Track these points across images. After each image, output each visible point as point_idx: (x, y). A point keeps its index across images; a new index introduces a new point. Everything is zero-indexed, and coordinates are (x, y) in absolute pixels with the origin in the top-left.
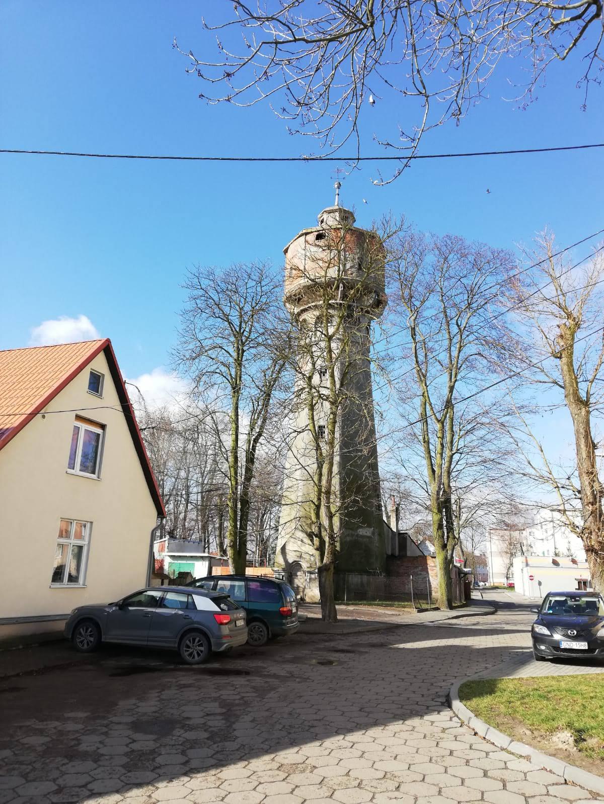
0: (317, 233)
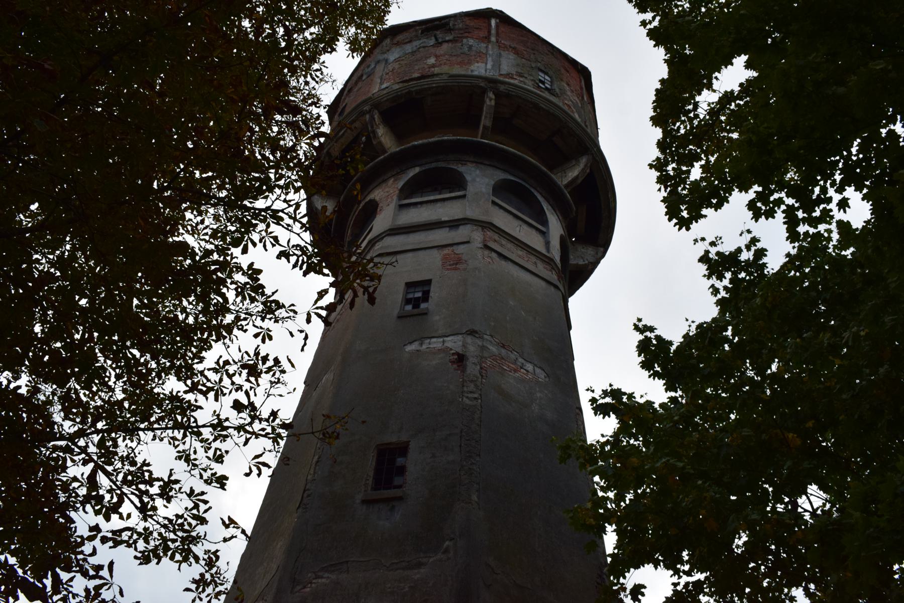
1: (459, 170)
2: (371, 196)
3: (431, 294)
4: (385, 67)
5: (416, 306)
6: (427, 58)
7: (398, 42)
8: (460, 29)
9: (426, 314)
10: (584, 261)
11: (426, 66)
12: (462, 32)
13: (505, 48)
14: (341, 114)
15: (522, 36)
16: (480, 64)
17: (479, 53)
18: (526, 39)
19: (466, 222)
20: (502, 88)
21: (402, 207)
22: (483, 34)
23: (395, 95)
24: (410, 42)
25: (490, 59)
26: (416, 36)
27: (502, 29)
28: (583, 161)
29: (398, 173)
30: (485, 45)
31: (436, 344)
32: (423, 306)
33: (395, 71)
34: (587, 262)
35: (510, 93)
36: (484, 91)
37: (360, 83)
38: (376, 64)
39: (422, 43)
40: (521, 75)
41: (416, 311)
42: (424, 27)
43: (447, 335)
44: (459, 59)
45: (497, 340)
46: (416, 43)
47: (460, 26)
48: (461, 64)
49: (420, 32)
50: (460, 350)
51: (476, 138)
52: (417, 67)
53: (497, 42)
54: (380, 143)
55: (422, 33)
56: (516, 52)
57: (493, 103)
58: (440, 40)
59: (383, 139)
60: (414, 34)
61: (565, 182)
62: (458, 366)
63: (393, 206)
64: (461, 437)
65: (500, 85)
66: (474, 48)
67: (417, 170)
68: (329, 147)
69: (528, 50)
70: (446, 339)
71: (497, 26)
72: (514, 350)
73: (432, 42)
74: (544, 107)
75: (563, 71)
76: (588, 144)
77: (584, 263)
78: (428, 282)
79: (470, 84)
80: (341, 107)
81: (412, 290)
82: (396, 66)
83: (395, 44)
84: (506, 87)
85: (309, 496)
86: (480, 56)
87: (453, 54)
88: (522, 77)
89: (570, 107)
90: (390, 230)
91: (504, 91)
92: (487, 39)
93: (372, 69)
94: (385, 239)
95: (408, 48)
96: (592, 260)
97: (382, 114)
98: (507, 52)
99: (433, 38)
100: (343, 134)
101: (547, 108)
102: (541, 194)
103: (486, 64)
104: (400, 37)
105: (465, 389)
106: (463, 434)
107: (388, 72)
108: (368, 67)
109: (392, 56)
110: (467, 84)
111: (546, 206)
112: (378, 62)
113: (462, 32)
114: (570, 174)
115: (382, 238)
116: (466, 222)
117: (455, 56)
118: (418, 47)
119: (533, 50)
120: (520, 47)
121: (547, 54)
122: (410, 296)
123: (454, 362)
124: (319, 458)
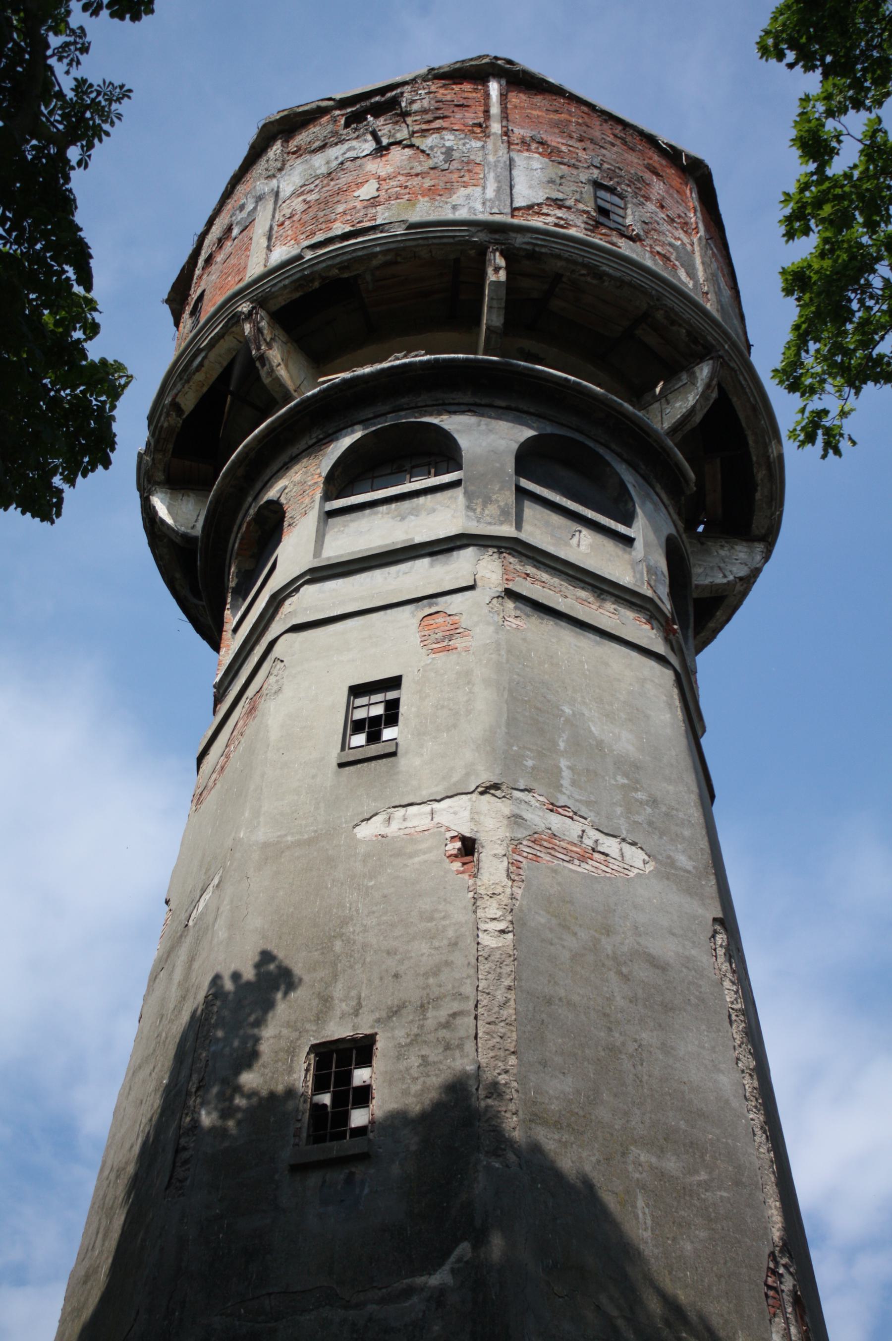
1: (446, 427)
2: (272, 494)
3: (403, 709)
4: (275, 209)
5: (374, 737)
6: (359, 185)
7: (299, 148)
8: (425, 111)
9: (394, 754)
10: (725, 576)
11: (359, 205)
12: (429, 117)
13: (525, 144)
14: (195, 312)
15: (556, 111)
16: (469, 190)
17: (468, 163)
18: (564, 116)
19: (465, 542)
20: (519, 240)
21: (332, 514)
22: (472, 117)
23: (299, 275)
24: (322, 148)
25: (491, 176)
26: (335, 133)
27: (517, 99)
28: (704, 371)
29: (320, 440)
30: (479, 144)
31: (418, 817)
32: (388, 733)
33: (296, 218)
34: (731, 578)
35: (537, 249)
36: (482, 253)
37: (229, 243)
38: (257, 202)
39: (349, 149)
40: (558, 203)
41: (375, 749)
42: (349, 110)
43: (438, 798)
44: (427, 183)
45: (541, 799)
46: (335, 153)
47: (425, 103)
48: (431, 192)
49: (343, 122)
50: (399, 980)
51: (475, 353)
52: (340, 208)
53: (506, 134)
54: (278, 380)
55: (347, 125)
56: (550, 152)
57: (502, 276)
58: (385, 141)
59: (282, 372)
60: (330, 127)
61: (666, 425)
62: (464, 864)
63: (313, 516)
64: (476, 1018)
65: (513, 235)
66: (456, 155)
67: (358, 435)
68: (175, 391)
69: (570, 143)
70: (436, 805)
71: (503, 96)
72: (575, 813)
73: (369, 145)
74: (611, 271)
75: (648, 176)
76: (709, 338)
77: (725, 581)
78: (395, 683)
79: (451, 240)
80: (194, 296)
81: (359, 701)
82: (298, 204)
83: (294, 153)
84: (528, 238)
85: (186, 1162)
86: (469, 171)
87: (414, 172)
88: (560, 207)
89: (668, 259)
90: (311, 571)
91: (524, 246)
92: (481, 128)
93: (249, 214)
94: (302, 589)
95: (319, 163)
96: (742, 572)
97: (280, 318)
98: (526, 154)
99: (369, 137)
100: (201, 365)
101: (618, 274)
102: (619, 455)
103: (484, 188)
104: (302, 138)
105: (480, 913)
106: (480, 1010)
107: (282, 219)
108: (242, 208)
109: (288, 183)
110: (445, 240)
111: (629, 478)
112: (259, 199)
113: (429, 117)
114: (678, 405)
115: (297, 590)
116: (465, 542)
117: (417, 175)
118: (340, 160)
119: (581, 140)
120: (555, 140)
121: (613, 145)
122: (360, 714)
123: (456, 856)
124: (201, 1081)
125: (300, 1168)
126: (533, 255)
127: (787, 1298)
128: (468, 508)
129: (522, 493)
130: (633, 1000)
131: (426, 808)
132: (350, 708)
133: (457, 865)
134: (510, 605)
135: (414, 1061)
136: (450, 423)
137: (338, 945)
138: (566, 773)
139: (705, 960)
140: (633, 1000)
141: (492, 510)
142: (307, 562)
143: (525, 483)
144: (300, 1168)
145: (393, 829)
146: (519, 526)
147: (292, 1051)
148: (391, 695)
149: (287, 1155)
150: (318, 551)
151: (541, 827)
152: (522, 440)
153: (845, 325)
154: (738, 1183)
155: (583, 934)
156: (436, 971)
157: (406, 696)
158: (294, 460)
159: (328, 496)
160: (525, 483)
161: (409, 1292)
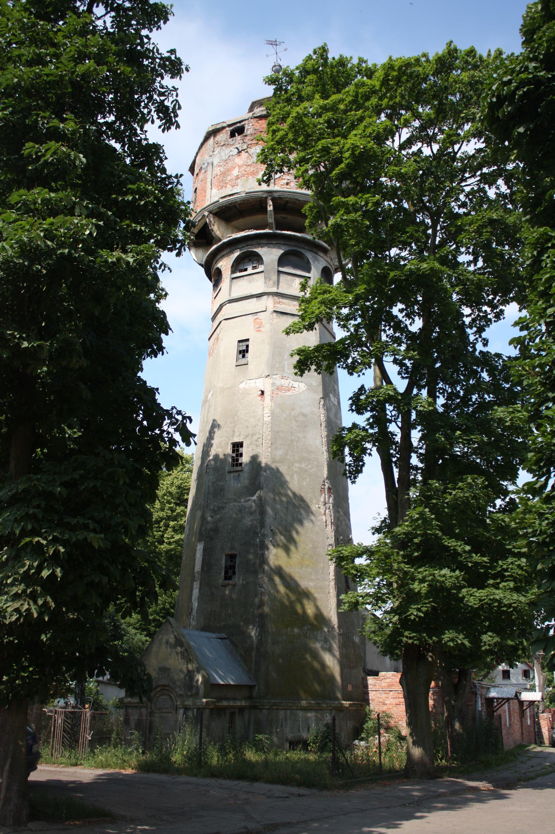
0: (231, 128)
20: (276, 195)
78: (247, 340)
122: (241, 349)
125: (230, 472)
126: (280, 198)
127: (326, 489)
128: (265, 283)
129: (279, 272)
130: (298, 427)
131: (254, 381)
132: (238, 346)
133: (260, 398)
134: (275, 314)
135: (250, 449)
136: (260, 251)
137: (236, 418)
138: (286, 366)
139: (316, 410)
140: (298, 427)
141: (271, 282)
142: (227, 298)
143: (281, 269)
144: (230, 472)
145: (247, 386)
146: (278, 288)
147: (227, 444)
148: (247, 343)
149: (227, 469)
150: (230, 295)
151: (279, 384)
152: (280, 255)
153: (316, 365)
154: (318, 466)
155: (287, 412)
156: (255, 427)
157: (250, 343)
158: (223, 256)
159: (233, 272)
160: (281, 269)
161: (249, 500)
